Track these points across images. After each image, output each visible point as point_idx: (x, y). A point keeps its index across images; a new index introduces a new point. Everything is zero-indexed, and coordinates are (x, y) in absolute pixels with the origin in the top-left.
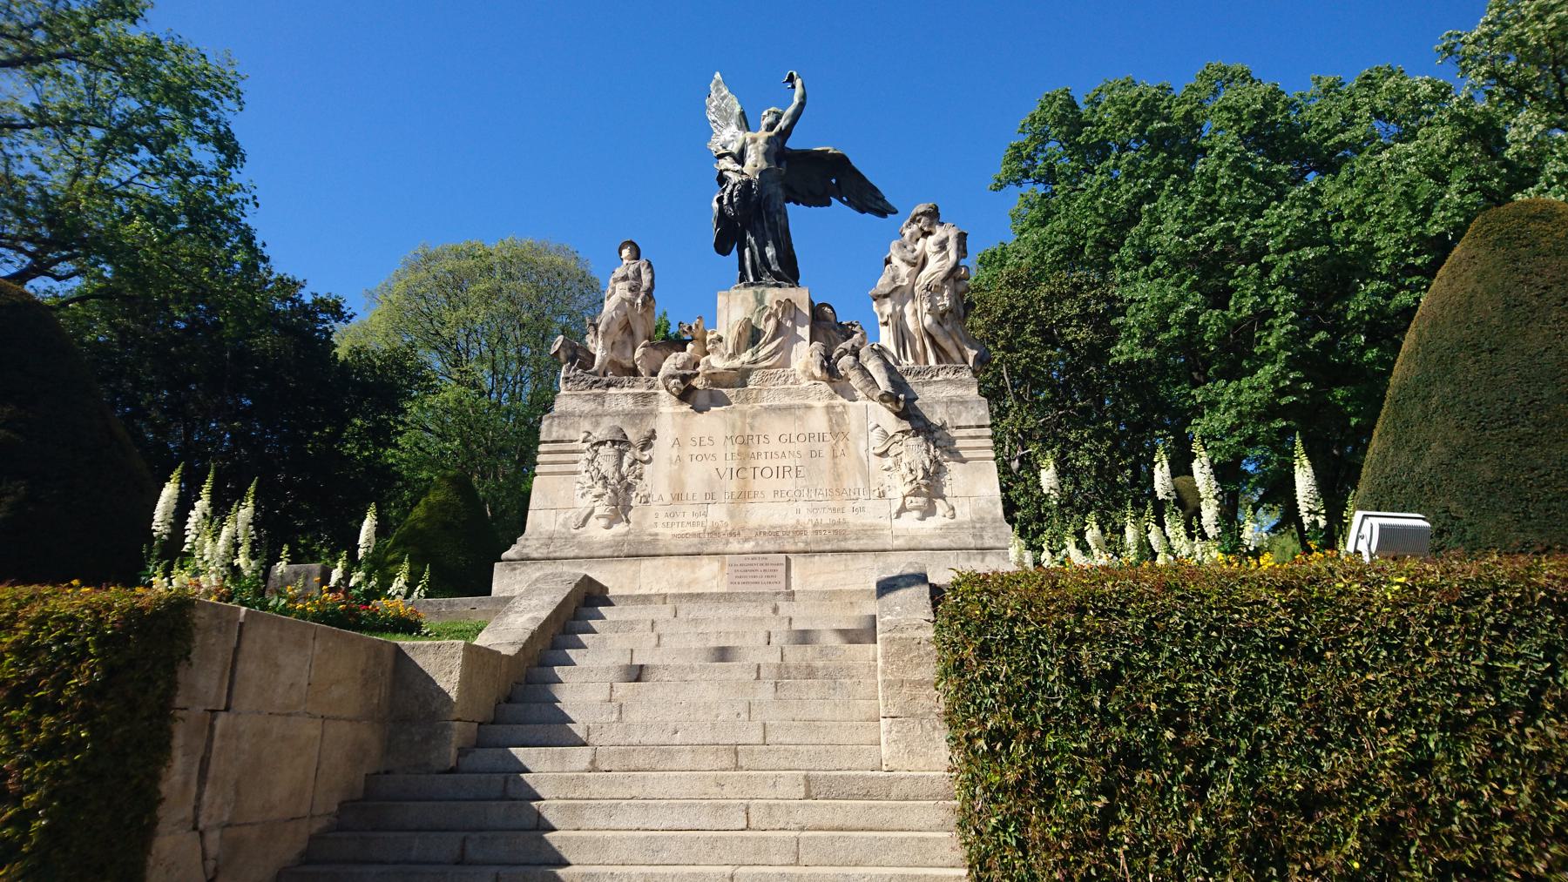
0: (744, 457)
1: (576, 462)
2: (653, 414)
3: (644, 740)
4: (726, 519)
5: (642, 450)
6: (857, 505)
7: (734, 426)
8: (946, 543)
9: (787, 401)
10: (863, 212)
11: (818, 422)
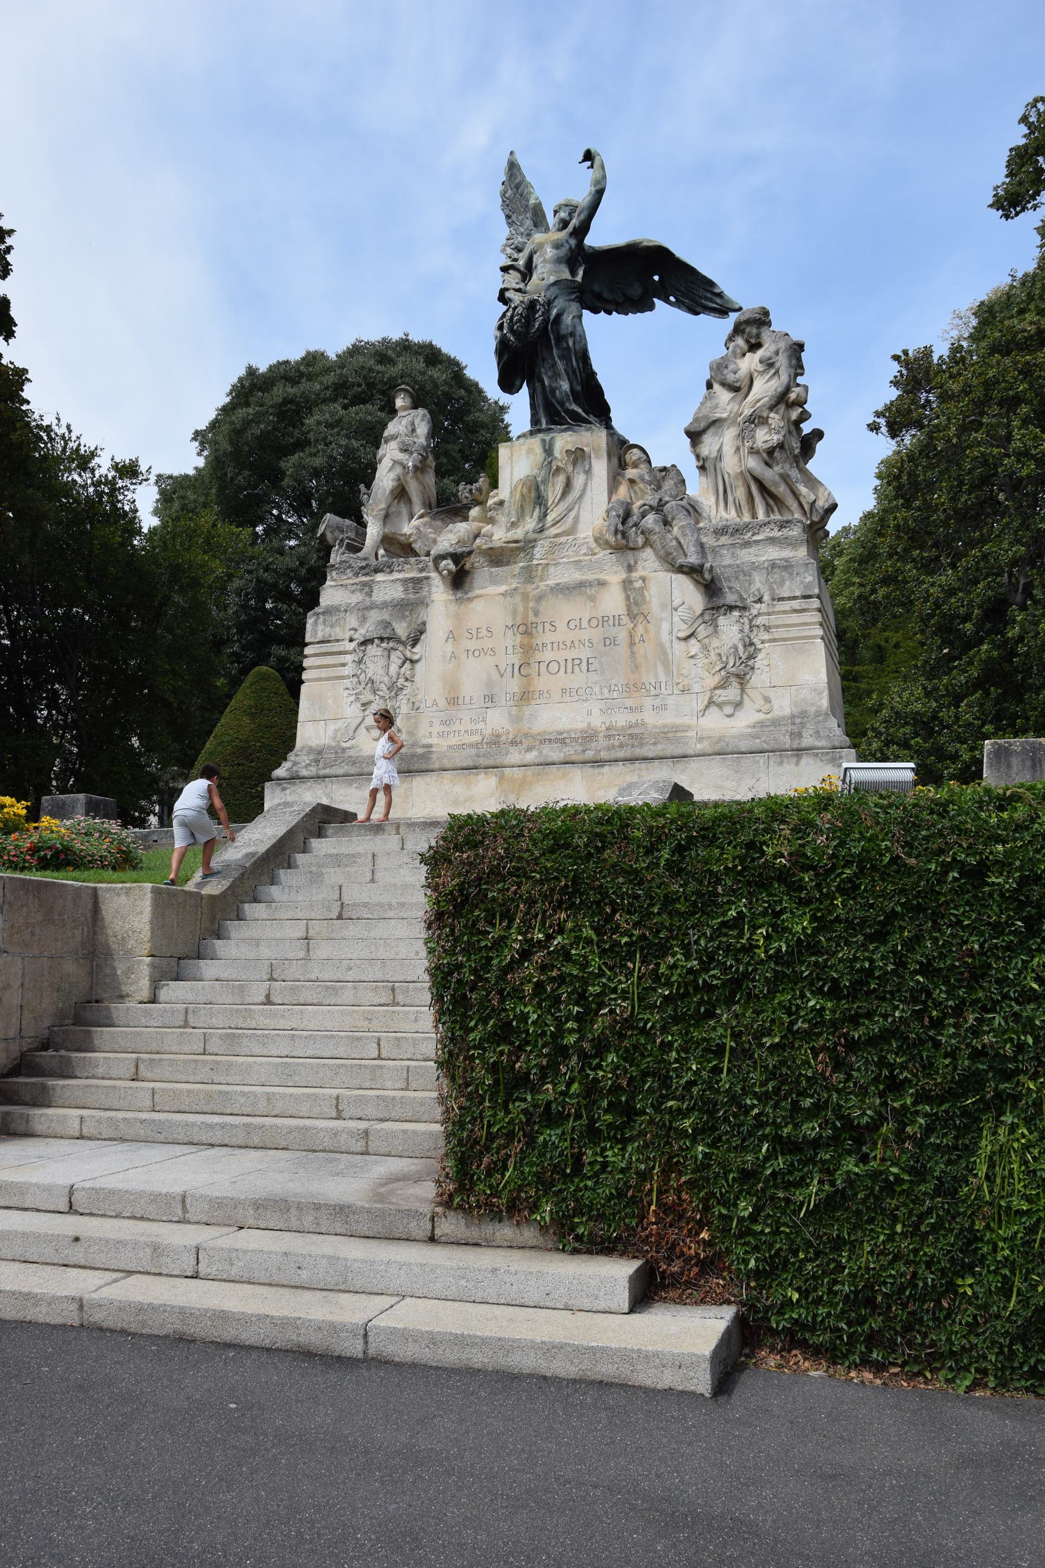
0: (528, 650)
1: (344, 665)
2: (423, 603)
3: (321, 977)
4: (507, 726)
5: (413, 646)
6: (657, 702)
7: (514, 613)
8: (757, 744)
9: (577, 576)
10: (696, 313)
11: (613, 601)
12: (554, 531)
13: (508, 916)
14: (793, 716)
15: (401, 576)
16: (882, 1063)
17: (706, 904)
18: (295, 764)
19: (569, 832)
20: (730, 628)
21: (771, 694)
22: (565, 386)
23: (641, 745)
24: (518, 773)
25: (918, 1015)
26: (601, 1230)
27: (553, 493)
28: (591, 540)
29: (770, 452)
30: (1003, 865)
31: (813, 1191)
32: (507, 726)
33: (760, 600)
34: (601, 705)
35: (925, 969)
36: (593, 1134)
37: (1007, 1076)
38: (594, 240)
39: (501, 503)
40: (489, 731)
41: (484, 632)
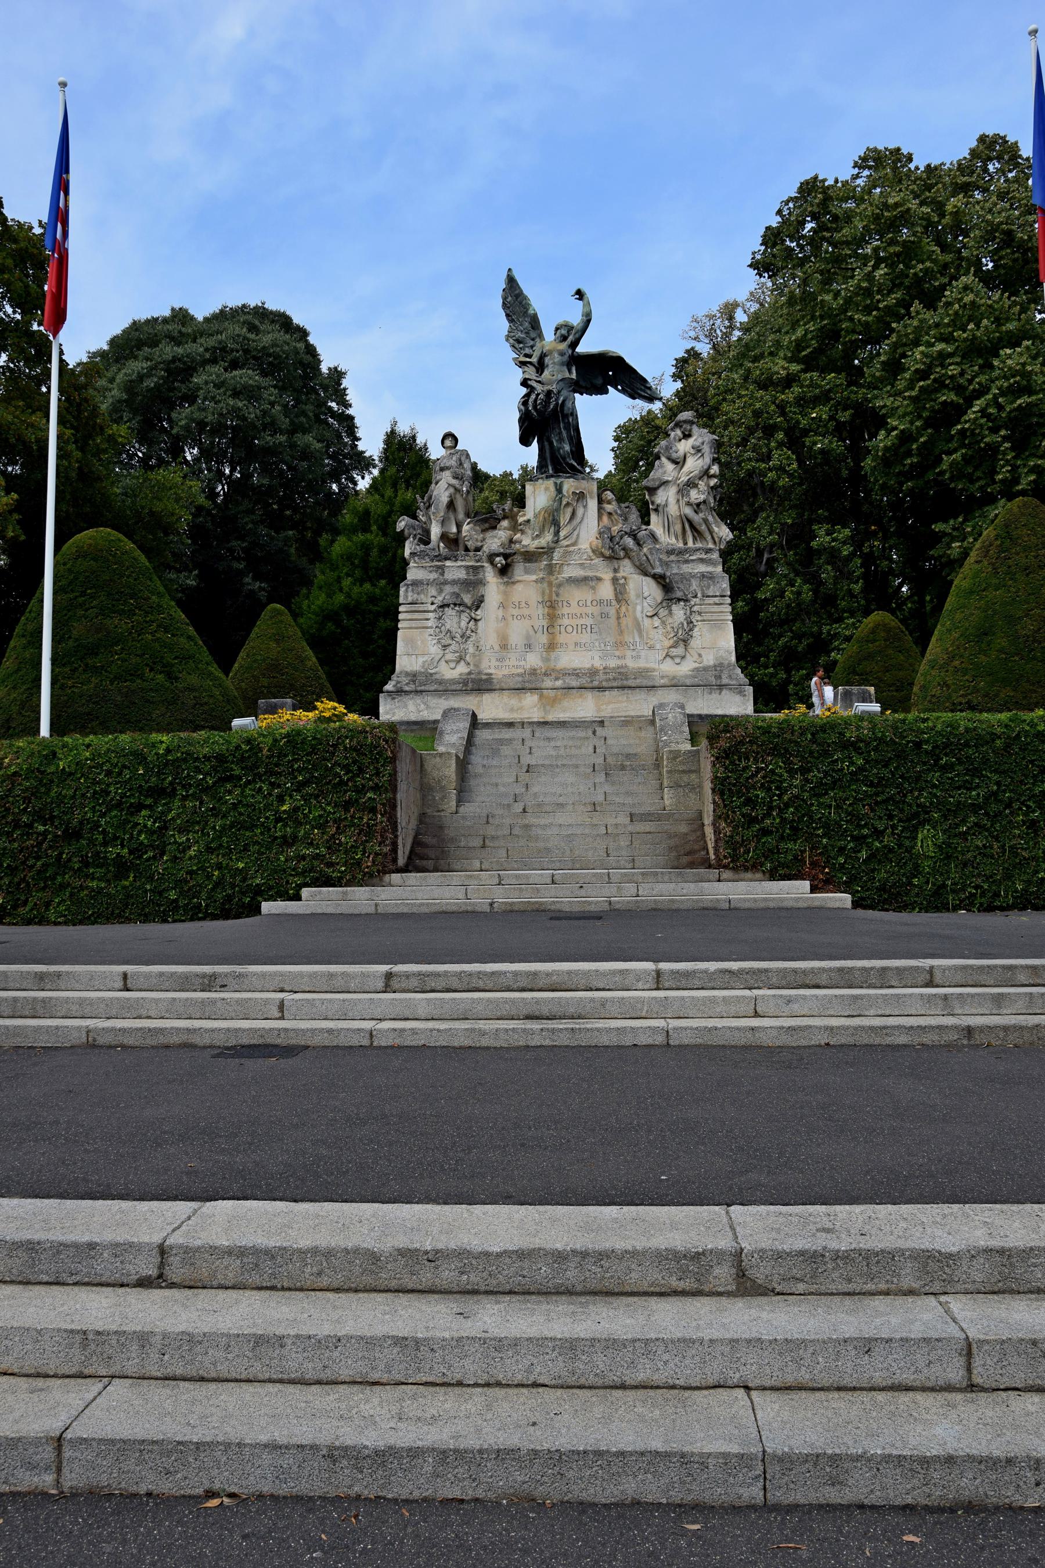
0: (552, 617)
1: (427, 619)
2: (482, 583)
4: (540, 664)
5: (476, 610)
6: (634, 653)
7: (543, 593)
11: (606, 591)
12: (565, 543)
13: (747, 758)
14: (715, 666)
15: (463, 563)
16: (887, 809)
17: (826, 754)
18: (398, 682)
19: (770, 727)
20: (679, 612)
21: (702, 652)
22: (567, 448)
23: (627, 679)
24: (552, 693)
25: (899, 793)
26: (788, 872)
27: (564, 518)
28: (589, 550)
29: (698, 505)
30: (927, 742)
31: (864, 854)
32: (540, 664)
33: (696, 597)
34: (600, 654)
35: (902, 777)
36: (782, 838)
37: (927, 813)
38: (581, 349)
39: (528, 521)
40: (528, 667)
41: (523, 605)
